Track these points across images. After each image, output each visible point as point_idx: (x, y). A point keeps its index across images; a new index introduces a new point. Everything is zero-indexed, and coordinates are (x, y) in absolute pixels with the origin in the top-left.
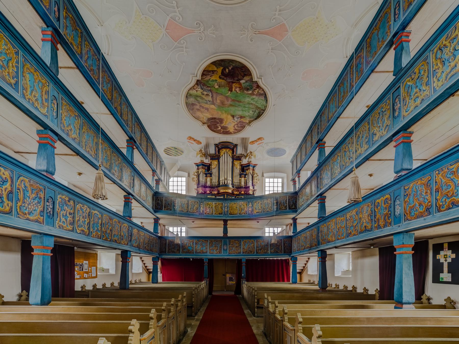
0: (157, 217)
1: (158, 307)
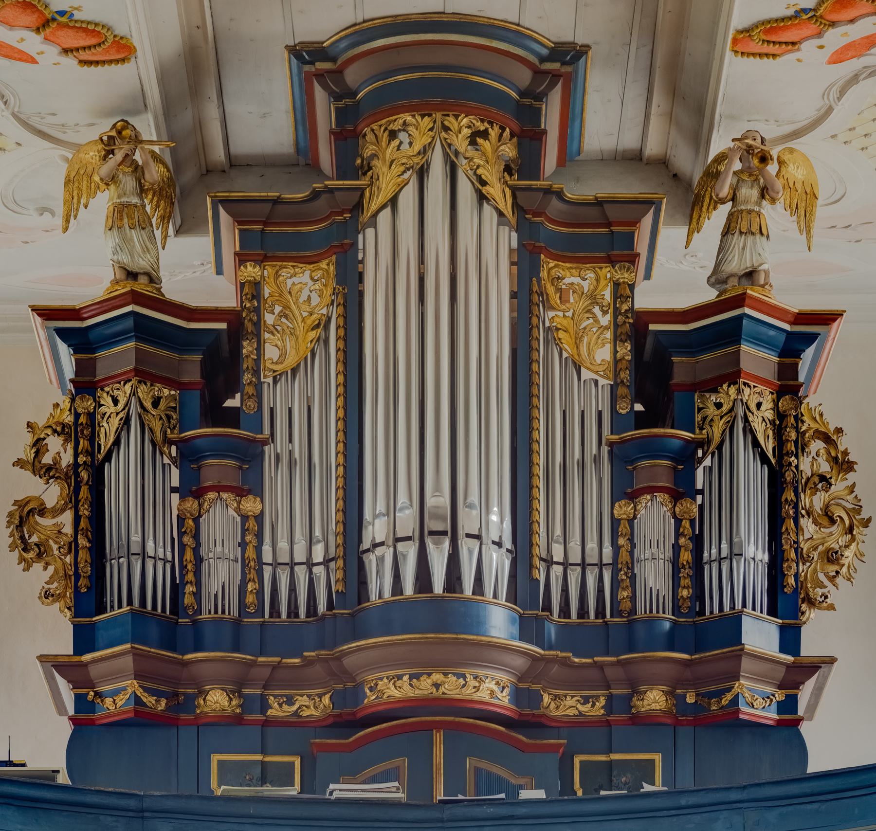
1: (570, 797)
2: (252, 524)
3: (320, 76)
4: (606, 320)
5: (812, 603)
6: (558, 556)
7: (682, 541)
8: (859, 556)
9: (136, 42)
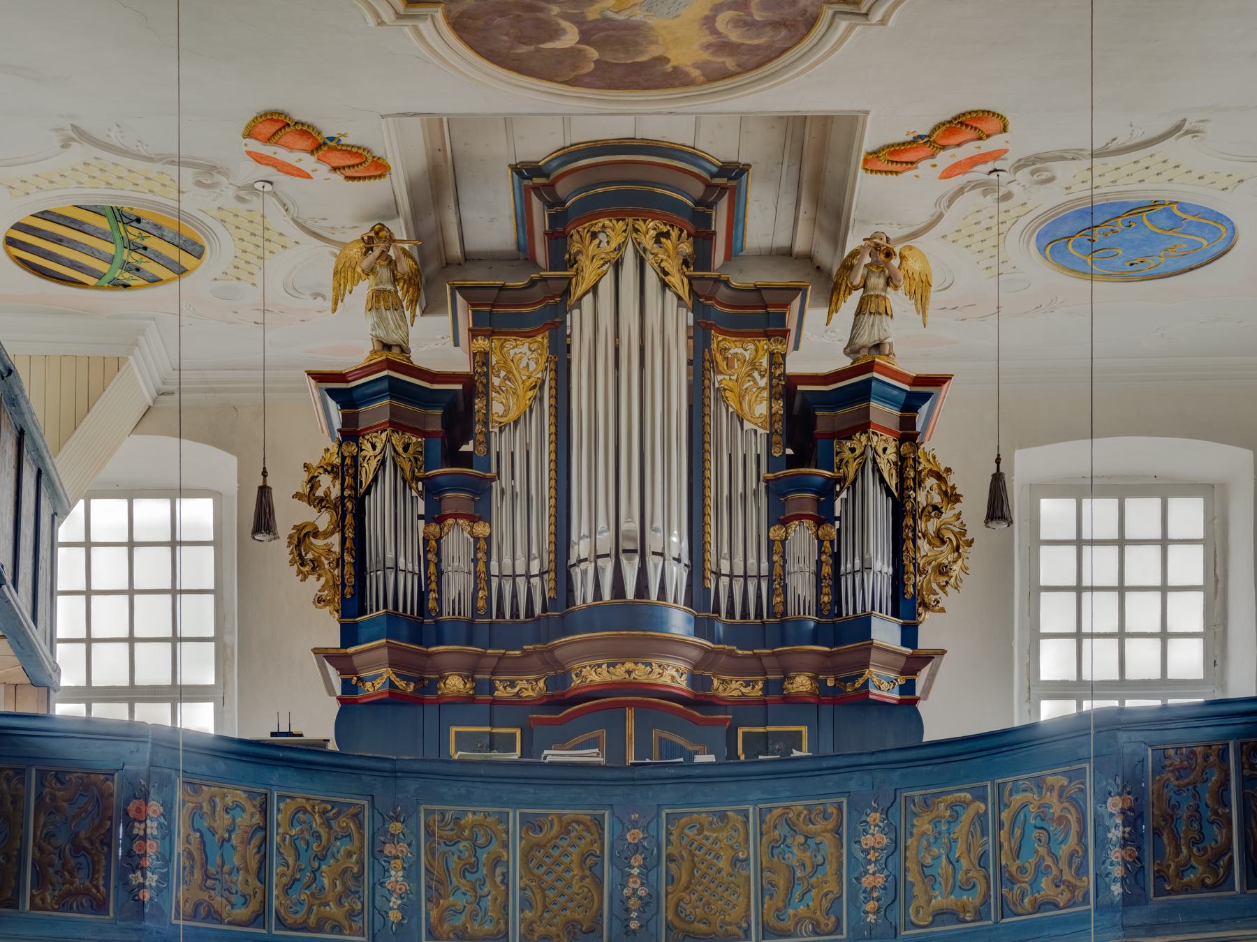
2: (482, 544)
3: (536, 189)
4: (763, 382)
6: (725, 569)
7: (824, 557)
8: (965, 569)
9: (390, 162)
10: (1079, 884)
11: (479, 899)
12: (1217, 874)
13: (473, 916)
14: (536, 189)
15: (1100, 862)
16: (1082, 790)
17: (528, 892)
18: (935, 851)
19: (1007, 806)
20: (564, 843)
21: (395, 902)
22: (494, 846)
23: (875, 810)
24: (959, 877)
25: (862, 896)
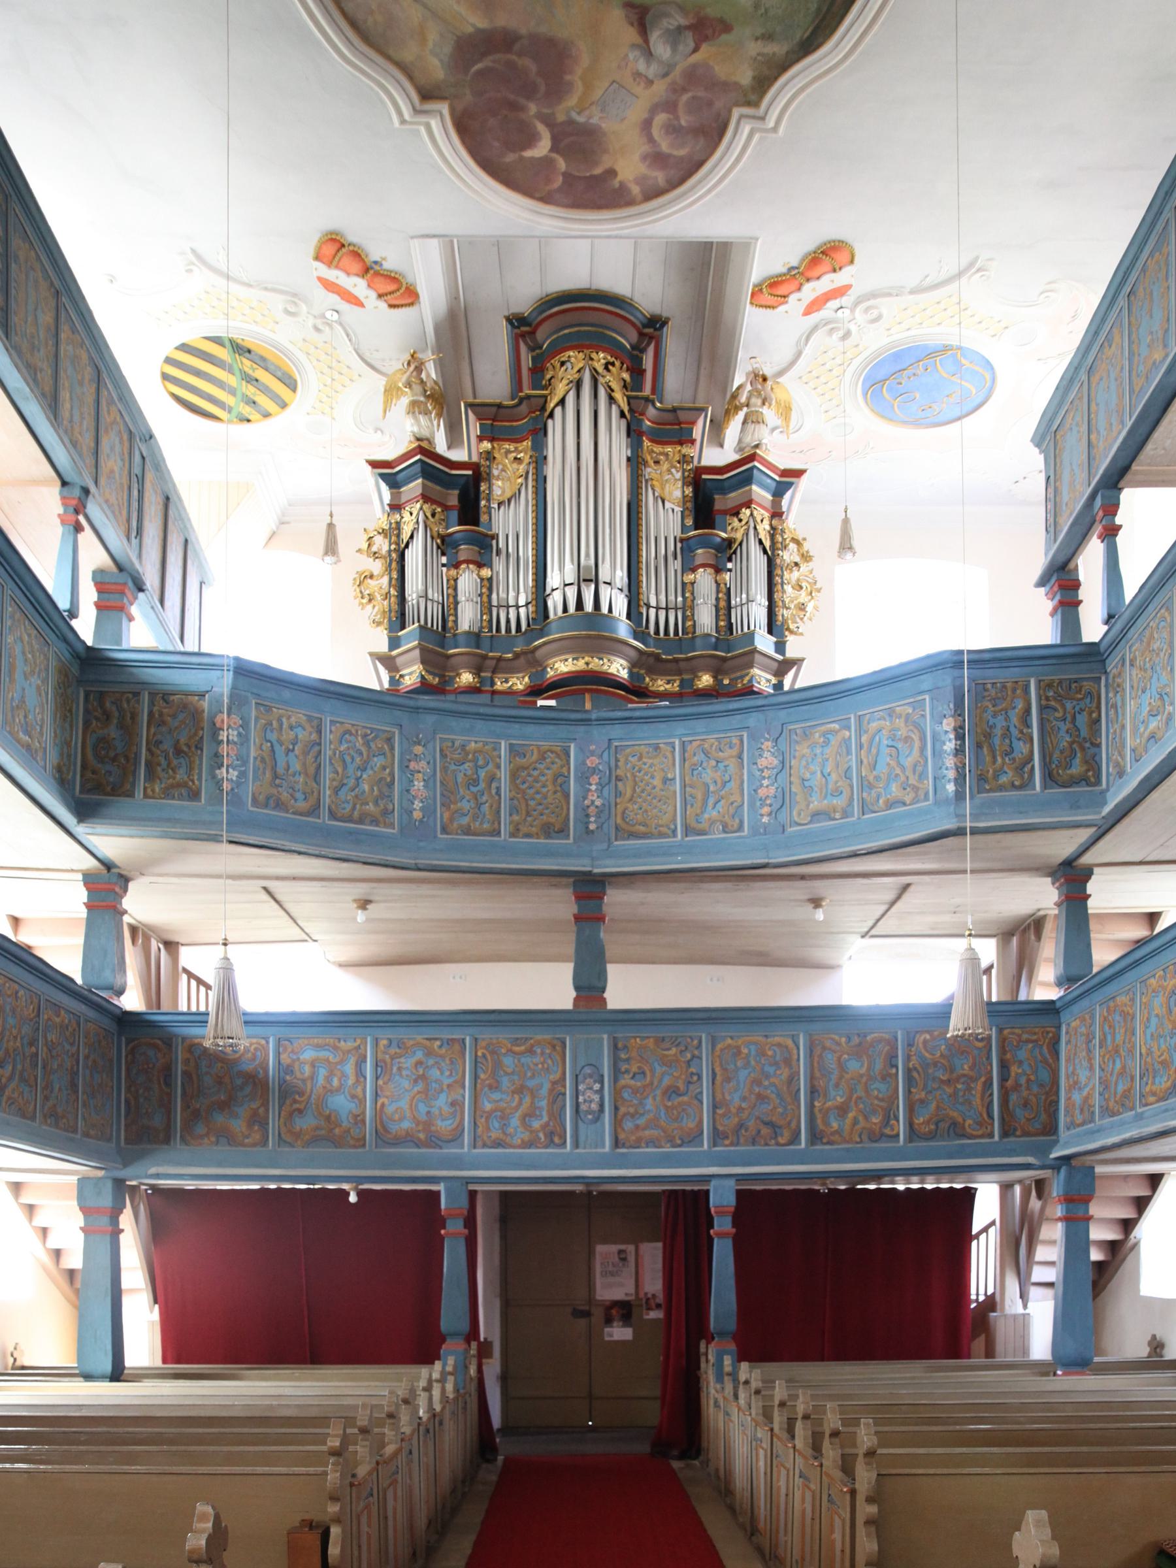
0: (108, 865)
2: (486, 583)
3: (523, 335)
4: (678, 475)
5: (792, 632)
6: (653, 603)
7: (720, 595)
8: (816, 608)
9: (419, 290)
10: (921, 786)
11: (479, 806)
12: (1023, 778)
13: (475, 817)
14: (523, 335)
15: (938, 767)
16: (923, 716)
17: (515, 802)
18: (812, 767)
19: (866, 732)
20: (542, 766)
21: (417, 805)
22: (490, 766)
23: (768, 740)
24: (830, 786)
25: (758, 803)
